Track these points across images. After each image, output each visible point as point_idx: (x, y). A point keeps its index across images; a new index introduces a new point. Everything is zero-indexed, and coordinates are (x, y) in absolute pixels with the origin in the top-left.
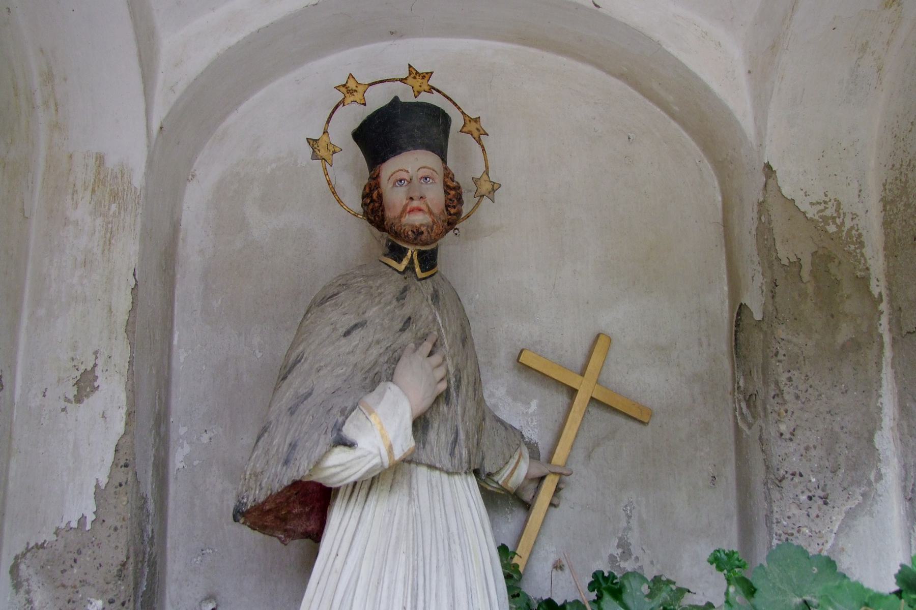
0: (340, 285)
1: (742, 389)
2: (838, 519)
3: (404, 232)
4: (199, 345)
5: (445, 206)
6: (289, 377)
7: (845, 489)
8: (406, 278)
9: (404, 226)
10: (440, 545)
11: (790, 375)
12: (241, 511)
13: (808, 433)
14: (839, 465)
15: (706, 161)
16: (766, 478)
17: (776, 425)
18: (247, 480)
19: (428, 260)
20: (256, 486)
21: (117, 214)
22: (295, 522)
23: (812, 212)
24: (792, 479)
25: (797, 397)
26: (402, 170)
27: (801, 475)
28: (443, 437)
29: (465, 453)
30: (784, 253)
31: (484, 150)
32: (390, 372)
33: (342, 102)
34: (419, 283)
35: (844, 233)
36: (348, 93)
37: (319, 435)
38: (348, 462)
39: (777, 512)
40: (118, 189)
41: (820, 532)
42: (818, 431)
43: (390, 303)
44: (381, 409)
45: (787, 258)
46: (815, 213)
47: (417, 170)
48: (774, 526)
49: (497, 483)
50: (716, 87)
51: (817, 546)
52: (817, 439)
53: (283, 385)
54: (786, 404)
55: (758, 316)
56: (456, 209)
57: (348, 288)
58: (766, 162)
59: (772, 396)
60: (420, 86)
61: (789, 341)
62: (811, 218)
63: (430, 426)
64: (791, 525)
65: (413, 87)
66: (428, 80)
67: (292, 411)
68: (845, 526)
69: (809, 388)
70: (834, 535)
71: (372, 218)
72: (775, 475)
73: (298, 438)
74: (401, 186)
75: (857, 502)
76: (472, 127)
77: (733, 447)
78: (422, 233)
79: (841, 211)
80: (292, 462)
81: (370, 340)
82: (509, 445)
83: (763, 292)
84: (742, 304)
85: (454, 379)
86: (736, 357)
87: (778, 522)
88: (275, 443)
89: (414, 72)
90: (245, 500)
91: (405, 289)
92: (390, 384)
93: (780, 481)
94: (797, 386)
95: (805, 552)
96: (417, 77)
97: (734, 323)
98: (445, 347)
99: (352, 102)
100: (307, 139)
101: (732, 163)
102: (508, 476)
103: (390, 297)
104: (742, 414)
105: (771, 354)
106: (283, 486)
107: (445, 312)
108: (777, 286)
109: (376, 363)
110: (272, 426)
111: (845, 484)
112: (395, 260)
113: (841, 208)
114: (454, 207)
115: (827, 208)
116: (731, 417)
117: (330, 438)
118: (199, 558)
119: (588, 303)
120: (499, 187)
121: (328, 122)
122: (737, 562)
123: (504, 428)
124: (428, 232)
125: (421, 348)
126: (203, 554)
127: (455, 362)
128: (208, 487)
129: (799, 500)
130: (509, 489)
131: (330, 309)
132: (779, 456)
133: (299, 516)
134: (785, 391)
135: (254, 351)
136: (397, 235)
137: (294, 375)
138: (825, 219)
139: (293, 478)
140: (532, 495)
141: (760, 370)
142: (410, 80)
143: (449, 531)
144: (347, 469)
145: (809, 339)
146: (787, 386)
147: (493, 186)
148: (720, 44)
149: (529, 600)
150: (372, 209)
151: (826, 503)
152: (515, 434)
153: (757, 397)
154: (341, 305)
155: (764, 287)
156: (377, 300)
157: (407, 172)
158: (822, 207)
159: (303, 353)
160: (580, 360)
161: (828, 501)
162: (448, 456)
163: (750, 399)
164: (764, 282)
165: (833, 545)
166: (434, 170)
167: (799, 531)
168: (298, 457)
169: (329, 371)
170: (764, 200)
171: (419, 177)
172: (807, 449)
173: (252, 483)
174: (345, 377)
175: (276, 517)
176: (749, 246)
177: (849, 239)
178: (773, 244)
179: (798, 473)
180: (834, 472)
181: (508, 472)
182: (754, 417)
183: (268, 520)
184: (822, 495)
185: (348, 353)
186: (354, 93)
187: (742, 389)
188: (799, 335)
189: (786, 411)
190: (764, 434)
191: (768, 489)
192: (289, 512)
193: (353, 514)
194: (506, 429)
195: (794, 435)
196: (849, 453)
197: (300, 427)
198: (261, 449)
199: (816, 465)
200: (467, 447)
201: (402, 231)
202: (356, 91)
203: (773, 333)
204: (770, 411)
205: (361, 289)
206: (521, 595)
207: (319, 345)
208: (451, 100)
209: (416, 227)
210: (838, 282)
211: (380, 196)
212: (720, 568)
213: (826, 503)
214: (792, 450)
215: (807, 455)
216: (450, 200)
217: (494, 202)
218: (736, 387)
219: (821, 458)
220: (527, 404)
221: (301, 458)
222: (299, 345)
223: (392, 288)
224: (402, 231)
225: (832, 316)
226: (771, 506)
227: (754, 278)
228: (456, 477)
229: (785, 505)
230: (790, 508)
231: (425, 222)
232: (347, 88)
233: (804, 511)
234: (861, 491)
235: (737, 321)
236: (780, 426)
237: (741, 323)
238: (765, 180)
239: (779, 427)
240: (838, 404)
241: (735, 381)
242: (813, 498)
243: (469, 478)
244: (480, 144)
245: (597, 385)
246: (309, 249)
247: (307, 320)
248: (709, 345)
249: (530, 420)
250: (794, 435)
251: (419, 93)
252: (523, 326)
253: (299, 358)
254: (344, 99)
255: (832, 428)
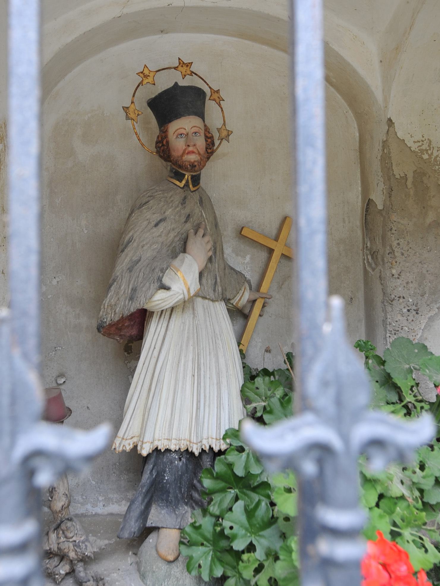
0: (149, 196)
1: (369, 248)
2: (424, 322)
3: (185, 166)
4: (49, 226)
5: (206, 148)
6: (126, 251)
7: (428, 305)
8: (184, 191)
9: (185, 162)
10: (211, 341)
11: (398, 241)
12: (103, 326)
13: (408, 274)
14: (425, 292)
15: (350, 112)
16: (383, 299)
17: (390, 270)
18: (106, 309)
19: (196, 180)
20: (112, 313)
21: (3, 150)
22: (125, 330)
23: (414, 147)
24: (399, 300)
25: (403, 254)
26: (182, 128)
27: (404, 298)
28: (210, 281)
29: (220, 289)
30: (397, 172)
31: (222, 110)
32: (180, 246)
33: (141, 83)
34: (192, 194)
35: (432, 159)
36: (144, 77)
37: (150, 284)
38: (166, 298)
39: (389, 318)
40: (3, 134)
41: (414, 329)
42: (414, 273)
43: (178, 206)
44: (183, 268)
45: (399, 174)
46: (417, 148)
47: (190, 128)
48: (388, 326)
49: (233, 304)
50: (361, 71)
51: (412, 337)
52: (413, 278)
53: (122, 255)
54: (396, 258)
55: (380, 207)
56: (211, 150)
57: (154, 198)
58: (389, 117)
59: (388, 253)
60: (186, 72)
61: (399, 222)
62: (414, 150)
63: (203, 275)
64: (398, 326)
65: (181, 73)
66: (190, 68)
67: (130, 270)
68: (428, 326)
69: (409, 249)
70: (422, 331)
71: (162, 155)
72: (388, 298)
73: (137, 285)
74: (182, 138)
75: (434, 312)
76: (215, 96)
77: (362, 281)
78: (195, 166)
79: (431, 146)
80: (135, 299)
81: (169, 228)
82: (239, 283)
83: (383, 193)
84: (370, 199)
85: (213, 248)
86: (366, 229)
87: (390, 324)
88: (122, 288)
89: (182, 63)
90: (105, 320)
91: (185, 198)
92: (186, 255)
93: (392, 301)
94: (402, 248)
95: (411, 342)
96: (184, 66)
97: (365, 210)
98: (208, 230)
99: (147, 83)
100: (123, 107)
101: (367, 115)
102: (238, 300)
103: (177, 203)
104: (368, 262)
105: (388, 229)
106: (131, 312)
107: (206, 210)
108: (392, 191)
109: (173, 241)
110: (118, 279)
111: (428, 303)
112: (179, 181)
113: (432, 144)
114: (210, 149)
115: (424, 144)
116: (361, 264)
117: (157, 285)
118: (54, 353)
119: (279, 198)
120: (232, 133)
121: (134, 96)
122: (370, 347)
123: (235, 273)
124: (199, 165)
125: (198, 233)
126: (56, 350)
127: (213, 238)
128: (57, 311)
129: (402, 312)
130: (239, 308)
131: (145, 211)
132: (392, 287)
133: (128, 327)
134: (395, 251)
135: (83, 230)
136: (180, 167)
137: (129, 249)
138: (422, 151)
139: (137, 308)
140: (249, 310)
141: (381, 238)
142: (180, 68)
143: (215, 333)
144: (165, 301)
145: (410, 221)
146: (397, 248)
147: (228, 133)
148: (364, 43)
149: (251, 369)
150: (163, 150)
151: (417, 313)
152: (241, 276)
153: (378, 253)
154: (151, 208)
155: (384, 191)
156: (170, 205)
157: (185, 129)
158: (420, 144)
159: (132, 236)
160: (274, 232)
161: (419, 312)
162: (212, 292)
163: (374, 254)
164: (384, 188)
165: (421, 336)
166: (200, 128)
167: (402, 329)
168: (139, 296)
169: (148, 247)
170: (387, 140)
171: (192, 132)
172: (407, 283)
173: (109, 310)
174: (157, 250)
175: (116, 328)
176: (376, 166)
177: (435, 163)
178: (391, 166)
179: (402, 296)
180: (422, 296)
181: (239, 298)
182: (376, 264)
183: (112, 330)
184: (415, 309)
185: (158, 236)
186: (148, 77)
187: (369, 248)
188: (404, 218)
189: (396, 262)
190: (382, 275)
191: (385, 305)
192: (123, 325)
193: (163, 325)
194: (237, 273)
195: (400, 276)
196: (431, 285)
197: (137, 279)
198: (113, 291)
199: (412, 292)
200: (221, 286)
201: (184, 165)
202: (149, 76)
203: (389, 218)
204: (386, 262)
205: (161, 198)
206: (246, 367)
207: (141, 232)
208: (203, 80)
209: (192, 162)
210: (428, 188)
211: (168, 142)
212: (361, 350)
213: (417, 313)
214: (399, 284)
215: (407, 286)
216: (208, 144)
217: (229, 143)
218: (365, 247)
219: (415, 289)
220: (244, 257)
221: (140, 297)
222: (130, 232)
223: (177, 198)
224: (184, 165)
225: (424, 208)
226: (386, 315)
227: (378, 185)
228: (217, 303)
229: (394, 315)
230: (397, 316)
231: (196, 159)
232: (144, 74)
233: (405, 318)
234: (437, 306)
235: (367, 208)
236: (392, 270)
237: (369, 210)
238: (388, 128)
239: (392, 271)
240: (425, 258)
241: (365, 243)
242: (410, 311)
243: (222, 302)
244: (220, 107)
245: (285, 247)
246: (113, 167)
247: (133, 217)
248: (349, 222)
249: (246, 267)
250: (400, 276)
251: (185, 76)
252: (241, 212)
253: (130, 240)
254: (142, 81)
255: (422, 271)
